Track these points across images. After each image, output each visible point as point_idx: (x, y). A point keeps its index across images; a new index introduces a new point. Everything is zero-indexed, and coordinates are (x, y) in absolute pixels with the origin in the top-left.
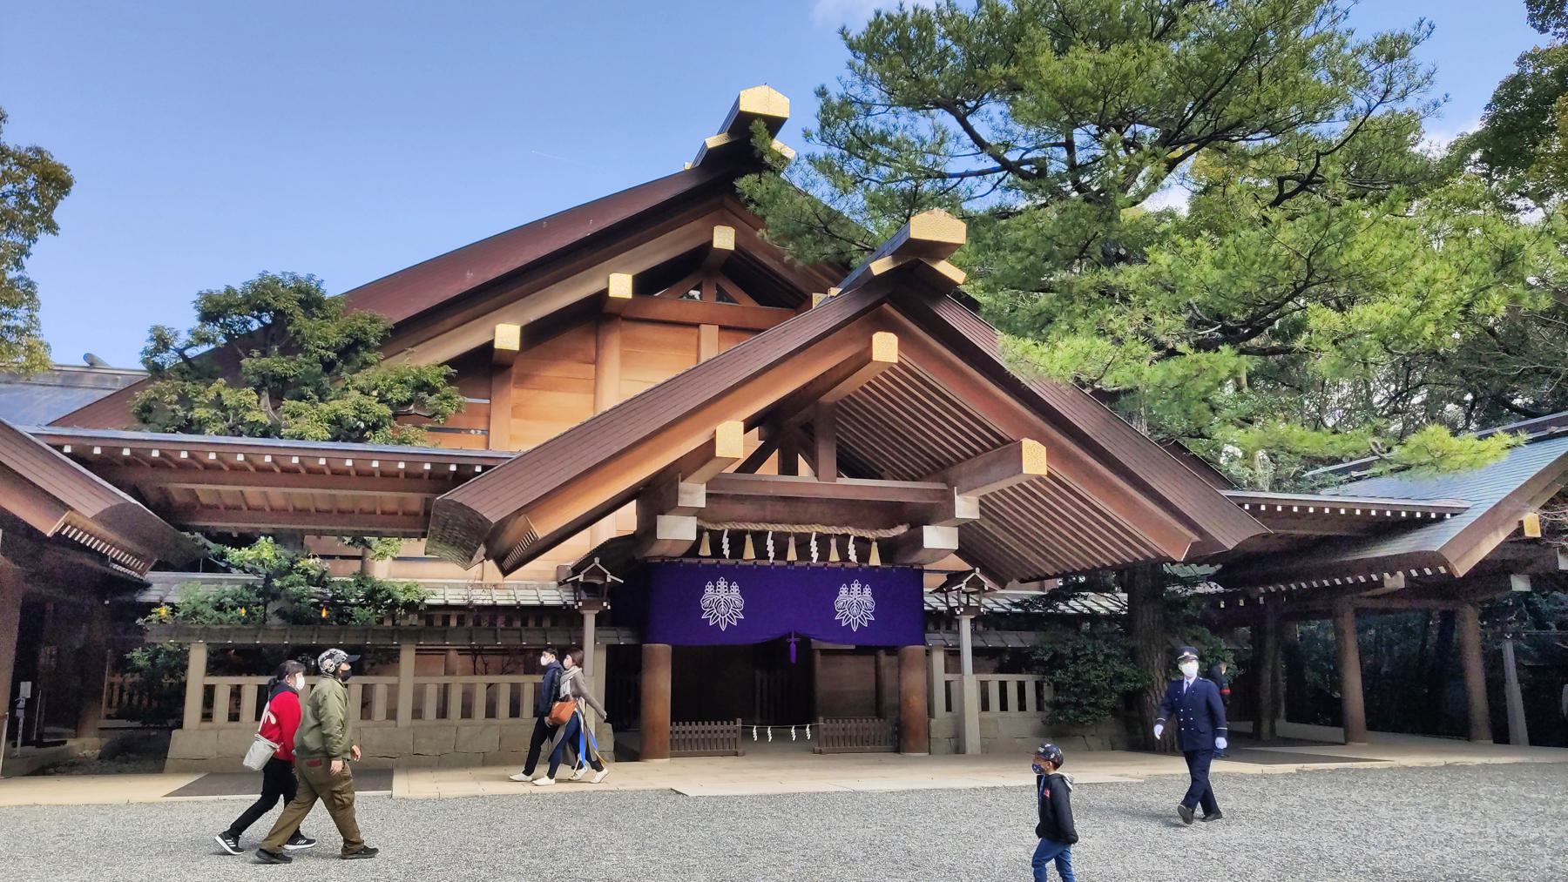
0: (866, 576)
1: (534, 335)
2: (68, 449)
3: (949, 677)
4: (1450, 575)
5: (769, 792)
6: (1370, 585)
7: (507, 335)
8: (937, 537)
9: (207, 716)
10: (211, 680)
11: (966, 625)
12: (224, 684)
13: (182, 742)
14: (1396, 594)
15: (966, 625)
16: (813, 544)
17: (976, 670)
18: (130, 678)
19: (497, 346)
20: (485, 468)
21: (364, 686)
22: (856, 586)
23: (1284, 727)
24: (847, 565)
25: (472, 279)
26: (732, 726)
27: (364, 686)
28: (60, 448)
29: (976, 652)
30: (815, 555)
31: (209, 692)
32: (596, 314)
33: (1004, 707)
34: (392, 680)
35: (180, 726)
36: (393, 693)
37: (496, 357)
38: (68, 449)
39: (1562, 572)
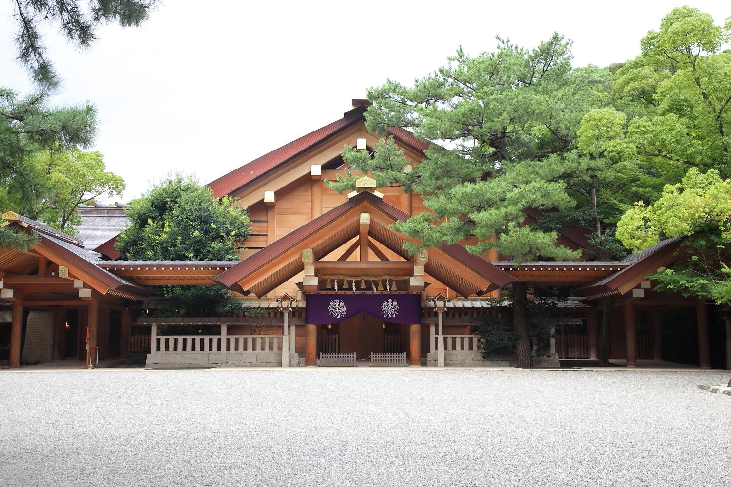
0: (394, 297)
1: (279, 194)
2: (108, 269)
4: (620, 294)
7: (269, 197)
9: (158, 349)
10: (229, 337)
12: (163, 338)
13: (150, 358)
19: (312, 174)
20: (228, 268)
21: (166, 339)
22: (390, 301)
25: (253, 175)
26: (403, 355)
27: (166, 339)
28: (105, 269)
31: (158, 341)
32: (308, 181)
34: (219, 337)
35: (150, 353)
36: (219, 340)
37: (313, 178)
38: (108, 269)
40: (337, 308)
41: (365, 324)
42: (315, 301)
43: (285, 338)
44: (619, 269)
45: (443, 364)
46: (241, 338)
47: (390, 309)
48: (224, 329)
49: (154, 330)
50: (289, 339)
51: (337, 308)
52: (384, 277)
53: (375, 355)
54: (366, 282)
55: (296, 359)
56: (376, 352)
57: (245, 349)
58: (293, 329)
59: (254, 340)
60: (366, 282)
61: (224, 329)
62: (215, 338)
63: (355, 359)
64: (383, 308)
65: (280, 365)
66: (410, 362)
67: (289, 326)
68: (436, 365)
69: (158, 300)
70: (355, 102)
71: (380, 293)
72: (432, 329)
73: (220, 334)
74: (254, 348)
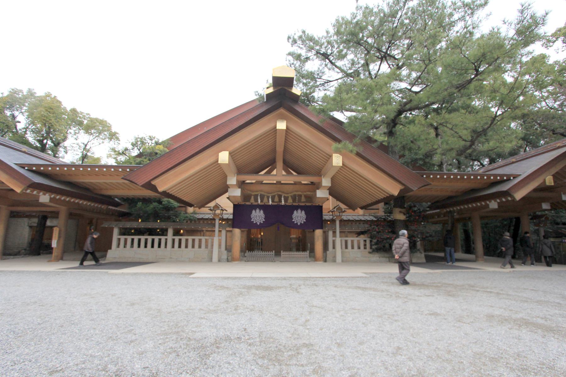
3: (334, 239)
5: (36, 151)
6: (482, 207)
8: (320, 194)
11: (338, 223)
12: (123, 238)
14: (494, 211)
15: (338, 223)
16: (259, 197)
17: (340, 237)
18: (161, 206)
23: (460, 255)
24: (280, 204)
26: (271, 253)
28: (24, 168)
29: (340, 232)
30: (259, 201)
33: (353, 248)
34: (166, 237)
38: (26, 168)
39: (564, 201)
40: (258, 216)
41: (279, 228)
42: (241, 212)
43: (216, 240)
44: (512, 178)
45: (340, 261)
46: (197, 238)
47: (299, 217)
48: (170, 232)
49: (116, 231)
50: (218, 240)
51: (258, 216)
52: (300, 193)
53: (284, 253)
54: (306, 197)
55: (225, 255)
56: (285, 250)
57: (186, 247)
58: (224, 232)
59: (193, 240)
60: (306, 197)
61: (170, 232)
62: (163, 238)
63: (308, 256)
64: (252, 216)
65: (210, 260)
66: (313, 257)
67: (220, 231)
68: (334, 261)
69: (94, 216)
70: (30, 91)
71: (276, 204)
72: (330, 233)
73: (166, 235)
74: (193, 246)
